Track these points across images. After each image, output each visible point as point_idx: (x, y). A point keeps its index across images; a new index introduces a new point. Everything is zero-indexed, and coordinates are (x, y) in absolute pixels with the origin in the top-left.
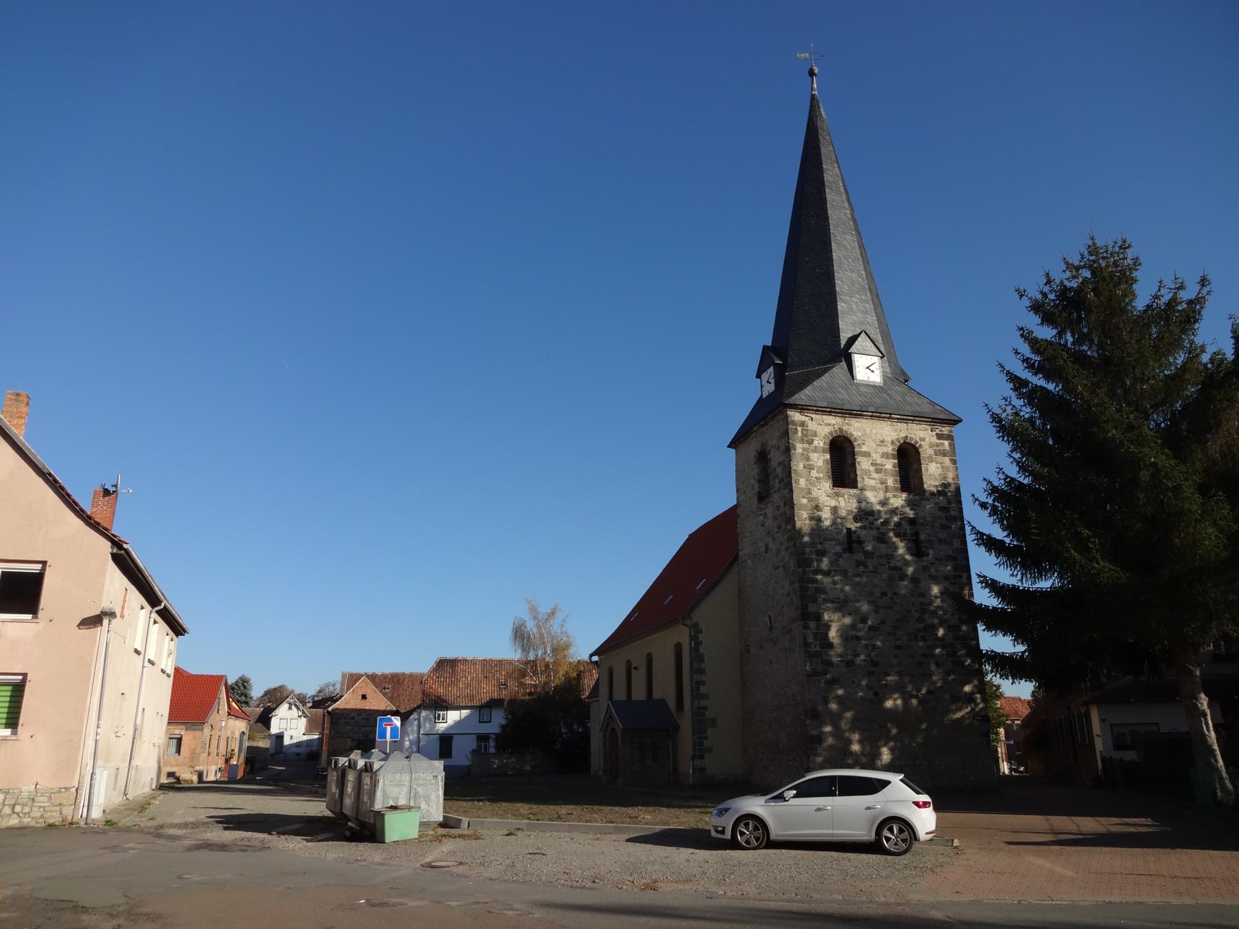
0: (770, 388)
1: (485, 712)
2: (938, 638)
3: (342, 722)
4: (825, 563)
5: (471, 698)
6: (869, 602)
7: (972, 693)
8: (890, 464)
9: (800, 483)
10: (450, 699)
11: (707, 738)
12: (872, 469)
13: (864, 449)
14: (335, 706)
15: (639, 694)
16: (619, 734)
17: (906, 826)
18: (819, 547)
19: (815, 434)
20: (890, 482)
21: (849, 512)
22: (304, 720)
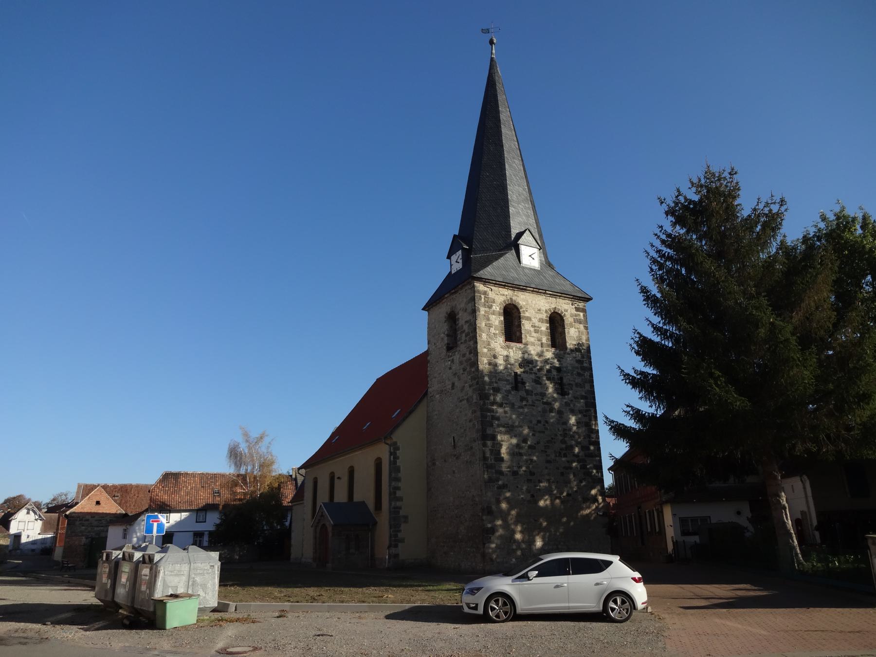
0: (459, 266)
1: (201, 514)
2: (575, 455)
3: (77, 523)
4: (499, 398)
5: (191, 503)
6: (529, 428)
7: (596, 495)
8: (544, 327)
9: (482, 337)
10: (173, 504)
11: (400, 531)
12: (532, 329)
13: (527, 314)
14: (72, 510)
15: (341, 496)
16: (330, 529)
17: (627, 598)
18: (495, 385)
19: (494, 301)
20: (544, 340)
21: (516, 361)
22: (40, 523)
